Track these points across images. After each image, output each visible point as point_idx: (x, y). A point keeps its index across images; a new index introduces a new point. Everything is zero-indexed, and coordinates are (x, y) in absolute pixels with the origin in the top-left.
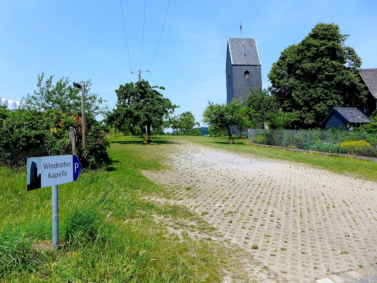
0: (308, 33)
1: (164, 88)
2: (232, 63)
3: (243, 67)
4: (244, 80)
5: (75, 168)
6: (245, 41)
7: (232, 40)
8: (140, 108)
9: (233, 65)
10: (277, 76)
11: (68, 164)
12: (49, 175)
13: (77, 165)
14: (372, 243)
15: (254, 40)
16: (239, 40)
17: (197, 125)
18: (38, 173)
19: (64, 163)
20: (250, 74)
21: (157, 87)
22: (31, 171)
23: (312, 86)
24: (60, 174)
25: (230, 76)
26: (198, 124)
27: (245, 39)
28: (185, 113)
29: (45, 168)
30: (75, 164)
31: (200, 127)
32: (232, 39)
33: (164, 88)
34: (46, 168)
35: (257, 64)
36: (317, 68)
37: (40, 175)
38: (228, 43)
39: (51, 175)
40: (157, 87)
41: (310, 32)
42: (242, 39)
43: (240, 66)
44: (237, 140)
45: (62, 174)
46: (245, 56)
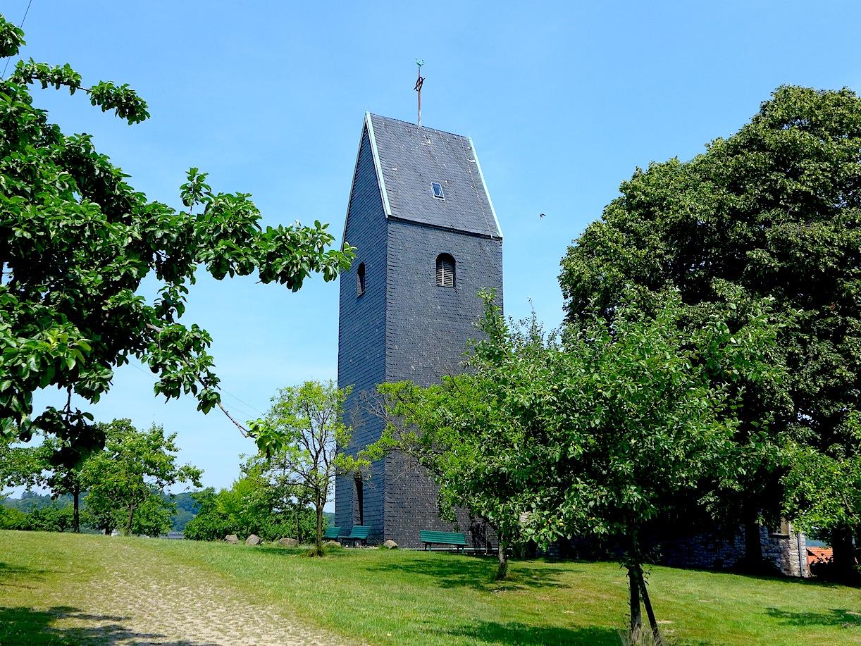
1: (131, 109)
2: (388, 211)
3: (432, 234)
4: (436, 290)
6: (435, 138)
7: (384, 124)
9: (392, 219)
15: (466, 143)
16: (410, 128)
17: (190, 482)
20: (458, 271)
21: (64, 79)
23: (819, 325)
25: (370, 266)
26: (195, 476)
27: (432, 131)
28: (105, 423)
31: (200, 490)
32: (385, 119)
33: (131, 109)
35: (487, 234)
36: (841, 248)
38: (366, 127)
40: (64, 79)
42: (423, 130)
43: (419, 230)
44: (793, 553)
46: (437, 191)
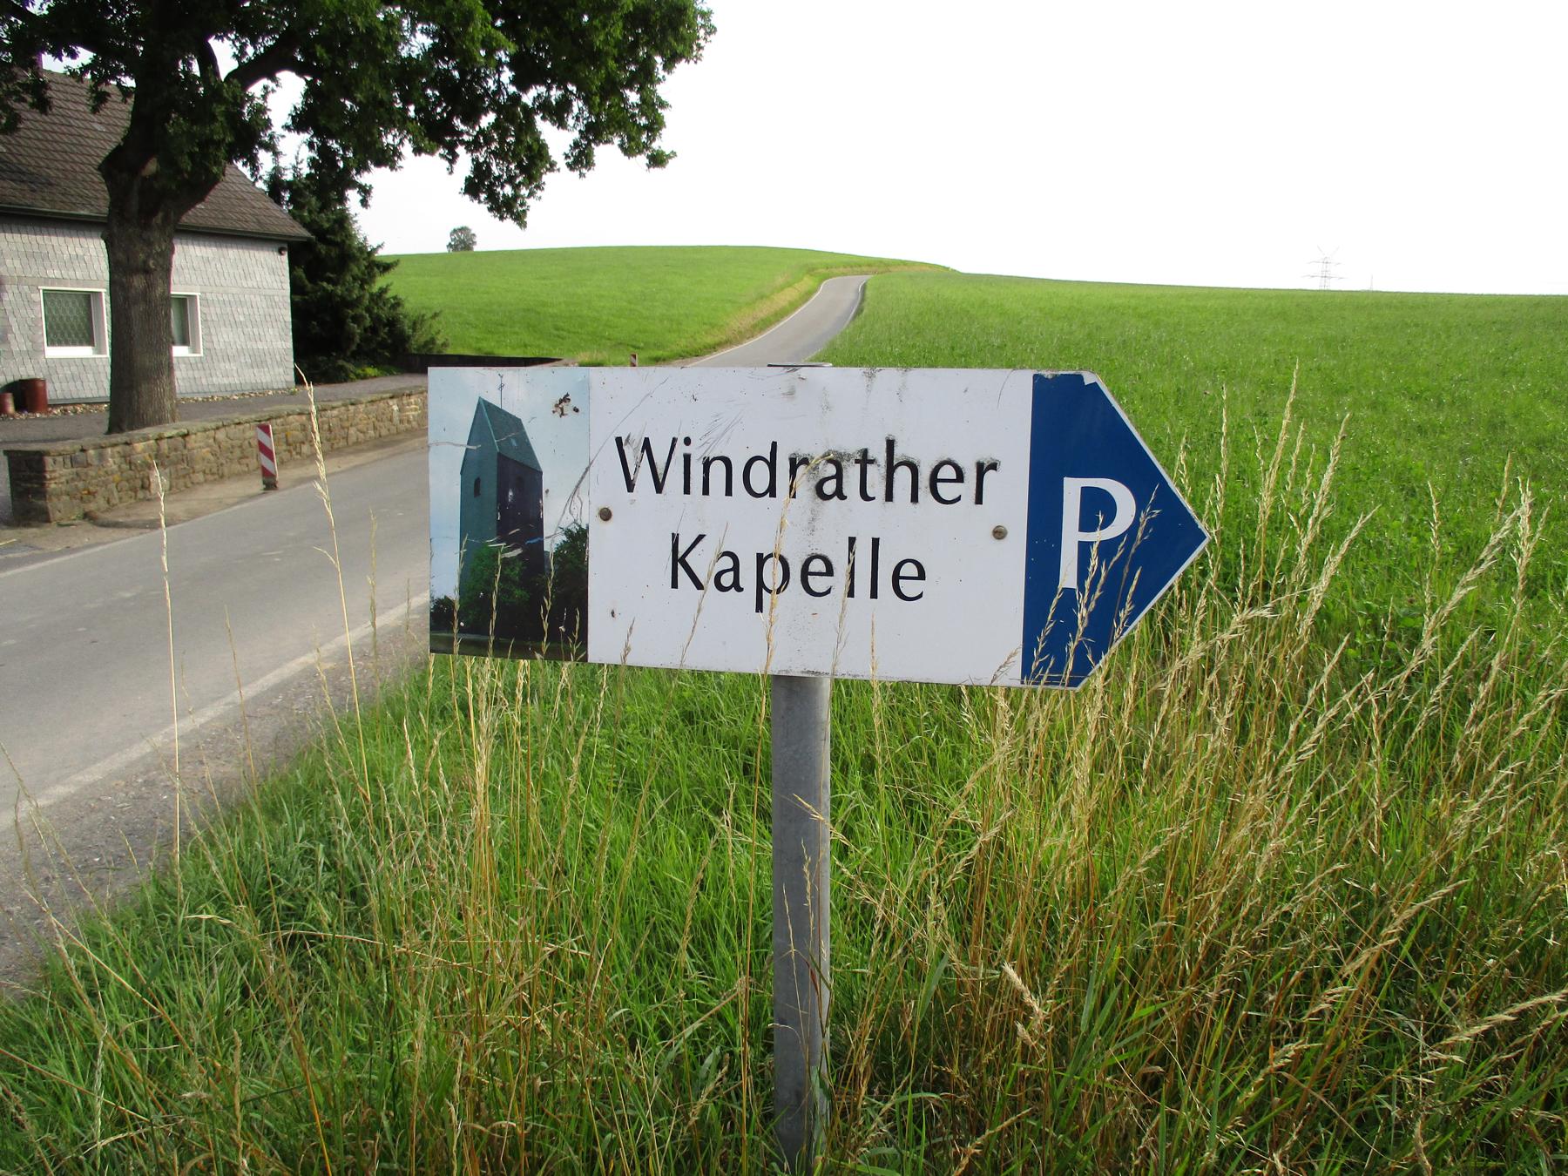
0: (451, 229)
5: (1071, 535)
8: (1187, 373)
10: (330, 1068)
11: (947, 472)
12: (679, 560)
13: (1097, 508)
14: (237, 839)
18: (555, 521)
19: (879, 453)
22: (472, 487)
24: (817, 566)
29: (630, 486)
30: (1072, 489)
33: (852, 541)
34: (644, 478)
37: (577, 540)
39: (702, 562)
41: (448, 240)
45: (841, 568)
